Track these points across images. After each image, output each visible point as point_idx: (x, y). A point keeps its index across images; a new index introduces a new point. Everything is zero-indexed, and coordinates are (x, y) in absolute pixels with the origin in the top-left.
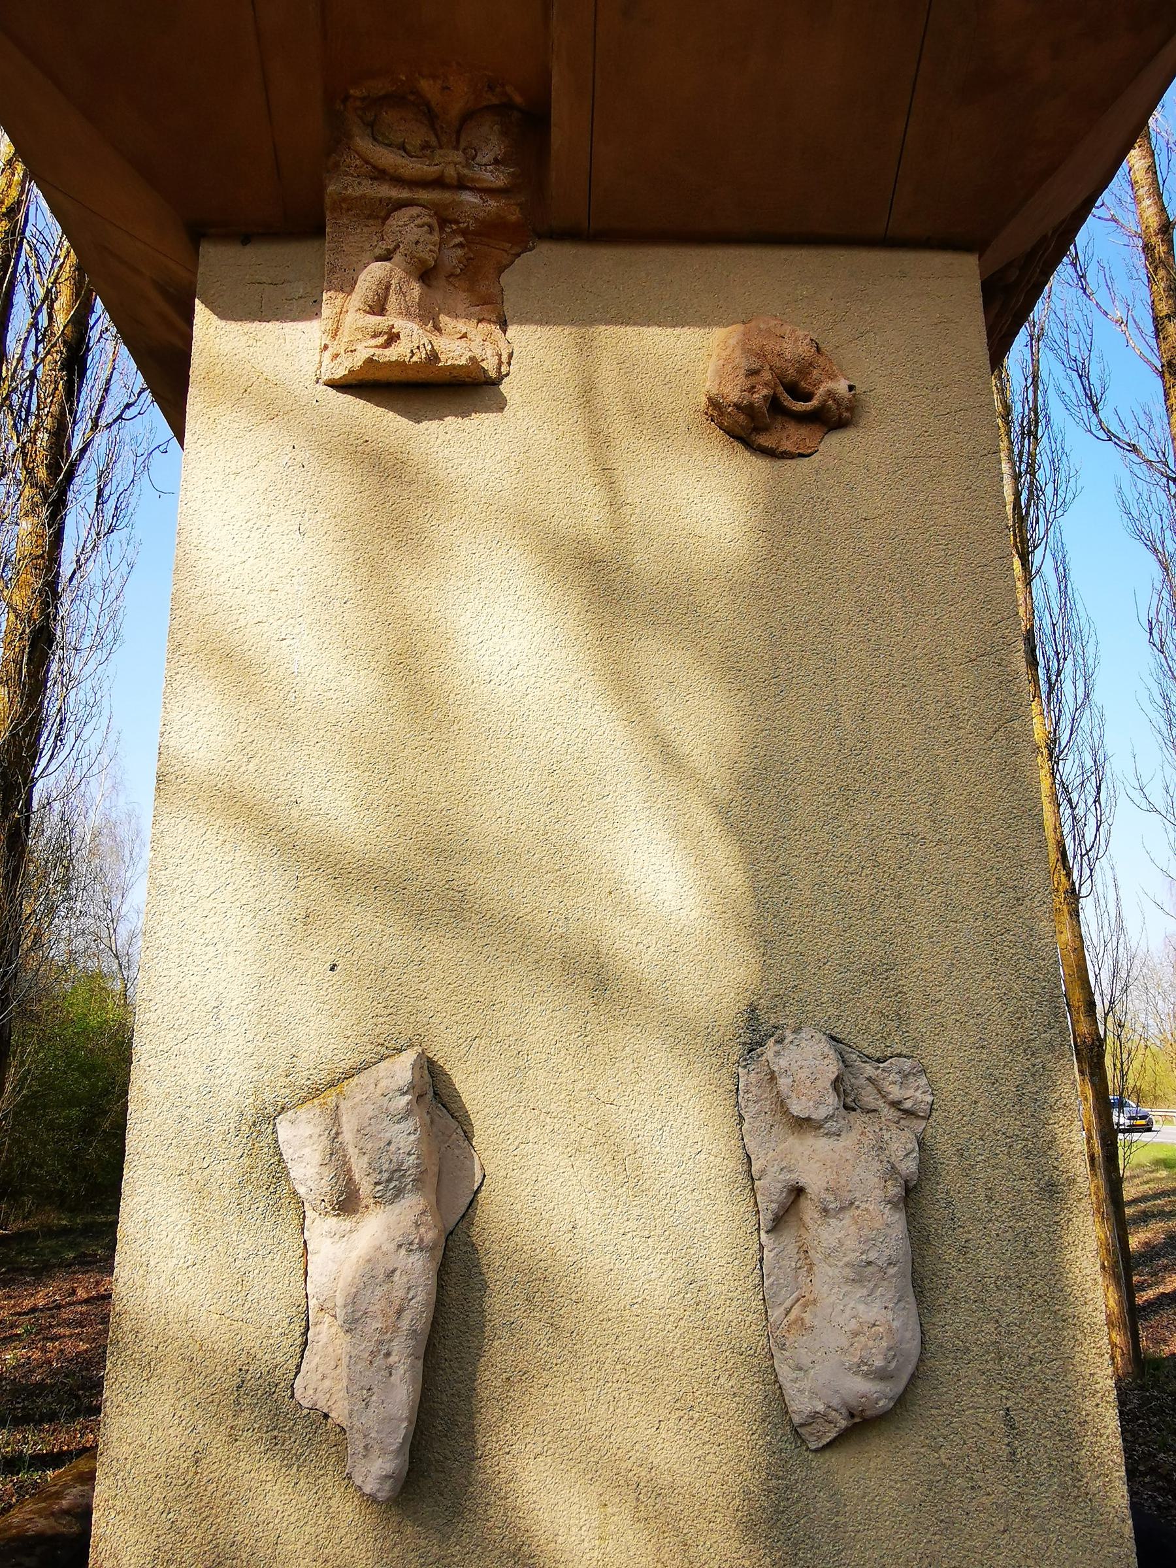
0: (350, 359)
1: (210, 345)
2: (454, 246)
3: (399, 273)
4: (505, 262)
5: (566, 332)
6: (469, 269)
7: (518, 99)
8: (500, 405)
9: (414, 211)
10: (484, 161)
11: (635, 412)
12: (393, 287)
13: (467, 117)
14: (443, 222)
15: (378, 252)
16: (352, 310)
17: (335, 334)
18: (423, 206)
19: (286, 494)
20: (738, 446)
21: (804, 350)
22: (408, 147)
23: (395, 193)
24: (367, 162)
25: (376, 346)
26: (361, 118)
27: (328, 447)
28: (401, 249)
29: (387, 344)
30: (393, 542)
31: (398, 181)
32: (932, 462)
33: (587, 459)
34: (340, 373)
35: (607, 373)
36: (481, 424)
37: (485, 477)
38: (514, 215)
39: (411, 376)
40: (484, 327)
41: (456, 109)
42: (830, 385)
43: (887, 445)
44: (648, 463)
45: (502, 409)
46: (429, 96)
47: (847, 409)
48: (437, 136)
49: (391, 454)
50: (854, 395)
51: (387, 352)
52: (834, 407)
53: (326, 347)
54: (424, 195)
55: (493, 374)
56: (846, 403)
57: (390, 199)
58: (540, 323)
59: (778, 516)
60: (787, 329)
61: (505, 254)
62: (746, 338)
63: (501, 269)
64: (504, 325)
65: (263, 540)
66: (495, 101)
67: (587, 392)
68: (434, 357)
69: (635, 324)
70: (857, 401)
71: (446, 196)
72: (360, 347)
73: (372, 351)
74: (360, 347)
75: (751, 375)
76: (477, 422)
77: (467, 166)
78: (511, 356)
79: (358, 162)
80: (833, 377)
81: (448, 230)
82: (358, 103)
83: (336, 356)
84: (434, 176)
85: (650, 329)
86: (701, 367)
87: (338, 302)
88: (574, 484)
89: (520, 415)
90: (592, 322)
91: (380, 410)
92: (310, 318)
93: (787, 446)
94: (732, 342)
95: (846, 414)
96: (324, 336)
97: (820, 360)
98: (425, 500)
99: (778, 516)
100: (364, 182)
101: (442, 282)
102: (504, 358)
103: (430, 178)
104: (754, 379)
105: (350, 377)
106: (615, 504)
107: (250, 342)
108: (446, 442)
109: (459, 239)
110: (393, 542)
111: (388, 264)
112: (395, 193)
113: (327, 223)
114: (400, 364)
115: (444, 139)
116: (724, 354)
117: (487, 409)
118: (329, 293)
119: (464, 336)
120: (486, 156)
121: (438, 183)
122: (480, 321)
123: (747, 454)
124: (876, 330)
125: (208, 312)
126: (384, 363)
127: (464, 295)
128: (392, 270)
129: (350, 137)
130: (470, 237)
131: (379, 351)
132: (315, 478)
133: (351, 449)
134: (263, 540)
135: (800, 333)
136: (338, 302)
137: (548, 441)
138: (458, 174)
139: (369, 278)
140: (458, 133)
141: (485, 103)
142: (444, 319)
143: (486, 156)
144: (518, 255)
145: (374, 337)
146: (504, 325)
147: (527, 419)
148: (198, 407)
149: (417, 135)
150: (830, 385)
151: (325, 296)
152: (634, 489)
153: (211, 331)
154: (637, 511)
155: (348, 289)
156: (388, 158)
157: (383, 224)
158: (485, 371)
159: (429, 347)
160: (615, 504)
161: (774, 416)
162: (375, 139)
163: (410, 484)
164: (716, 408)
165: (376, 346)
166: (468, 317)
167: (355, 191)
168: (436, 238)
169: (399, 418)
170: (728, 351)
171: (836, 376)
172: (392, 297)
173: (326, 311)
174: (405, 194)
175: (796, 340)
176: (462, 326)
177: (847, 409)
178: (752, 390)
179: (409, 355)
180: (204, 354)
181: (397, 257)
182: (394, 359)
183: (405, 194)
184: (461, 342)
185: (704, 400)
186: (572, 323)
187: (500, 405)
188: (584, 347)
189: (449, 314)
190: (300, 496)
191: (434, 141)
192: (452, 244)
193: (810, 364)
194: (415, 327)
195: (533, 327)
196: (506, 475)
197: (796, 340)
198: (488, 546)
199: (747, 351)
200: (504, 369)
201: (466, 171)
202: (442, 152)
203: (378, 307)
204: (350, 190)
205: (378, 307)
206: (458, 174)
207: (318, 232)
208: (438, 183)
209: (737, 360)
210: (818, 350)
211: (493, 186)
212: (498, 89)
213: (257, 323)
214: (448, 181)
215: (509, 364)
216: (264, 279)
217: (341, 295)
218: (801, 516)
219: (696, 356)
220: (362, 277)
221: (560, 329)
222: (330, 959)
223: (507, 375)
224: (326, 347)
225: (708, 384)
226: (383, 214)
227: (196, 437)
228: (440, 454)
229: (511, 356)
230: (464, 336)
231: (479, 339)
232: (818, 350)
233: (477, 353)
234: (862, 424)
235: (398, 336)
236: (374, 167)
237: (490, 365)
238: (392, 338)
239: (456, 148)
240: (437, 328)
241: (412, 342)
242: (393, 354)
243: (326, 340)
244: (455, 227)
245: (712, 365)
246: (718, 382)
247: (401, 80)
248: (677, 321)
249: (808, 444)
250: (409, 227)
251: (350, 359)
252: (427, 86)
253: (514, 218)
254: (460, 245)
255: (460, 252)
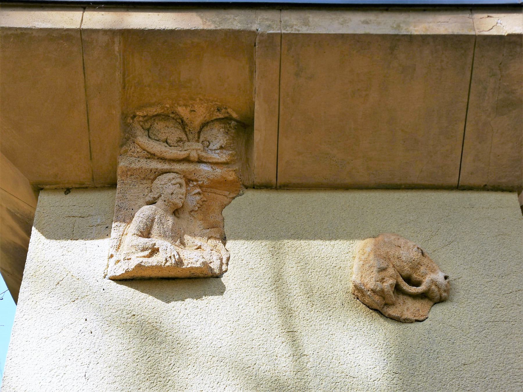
0: (127, 264)
1: (38, 255)
2: (195, 194)
3: (160, 212)
4: (225, 203)
5: (263, 244)
6: (202, 210)
7: (234, 115)
8: (221, 290)
9: (171, 176)
10: (214, 148)
11: (309, 293)
12: (156, 220)
13: (204, 125)
14: (188, 181)
15: (148, 199)
16: (130, 234)
17: (118, 248)
18: (177, 173)
19: (79, 351)
20: (375, 315)
21: (414, 255)
22: (169, 141)
23: (161, 166)
24: (144, 150)
25: (144, 257)
26: (142, 126)
27: (109, 319)
28: (162, 197)
29: (151, 255)
30: (148, 383)
31: (163, 159)
32: (504, 325)
33: (277, 325)
34: (119, 272)
35: (291, 270)
36: (210, 302)
37: (210, 338)
38: (231, 176)
39: (166, 274)
40: (212, 242)
41: (198, 121)
42: (433, 276)
43: (474, 314)
44: (318, 327)
45: (222, 293)
46: (183, 115)
47: (445, 291)
48: (187, 135)
49: (150, 323)
50: (448, 282)
51: (150, 260)
52: (436, 290)
53: (112, 256)
54: (177, 167)
55: (217, 271)
56: (443, 287)
57: (157, 169)
58: (247, 238)
59: (405, 362)
60: (402, 241)
61: (225, 198)
62: (377, 253)
63: (223, 206)
64: (224, 240)
65: (60, 384)
66: (221, 116)
67: (278, 282)
68: (180, 262)
69: (307, 238)
70: (450, 285)
71: (191, 167)
72: (133, 257)
73: (141, 259)
74: (133, 257)
75: (381, 271)
76: (206, 301)
77: (204, 150)
78: (228, 259)
79: (139, 150)
80: (433, 271)
81: (191, 185)
82: (141, 119)
83: (119, 261)
84: (184, 157)
85: (315, 242)
86: (349, 264)
87: (121, 229)
88: (269, 342)
89: (233, 297)
90: (279, 237)
91: (144, 295)
92: (103, 238)
93: (408, 315)
94: (368, 249)
95: (444, 294)
96: (111, 249)
97: (425, 261)
98: (171, 354)
99: (405, 362)
100: (142, 160)
101: (187, 215)
102: (224, 261)
103: (181, 158)
104: (383, 274)
105: (126, 275)
106: (298, 354)
107: (64, 253)
108: (184, 313)
109: (198, 190)
110: (148, 383)
111: (153, 207)
112: (161, 166)
113: (118, 183)
114: (158, 267)
115: (191, 136)
116: (363, 257)
117: (213, 294)
118: (116, 224)
119: (199, 248)
120: (215, 145)
121: (187, 160)
122: (209, 238)
123: (382, 320)
124: (458, 240)
125: (39, 235)
126: (148, 267)
127: (199, 223)
128: (156, 210)
129: (135, 137)
130: (204, 189)
131: (145, 260)
132: (98, 340)
133: (124, 320)
134: (60, 384)
135: (411, 244)
136: (121, 229)
137: (252, 314)
138: (198, 155)
139: (141, 215)
140: (199, 133)
141: (215, 118)
142: (187, 237)
143: (215, 145)
144: (234, 198)
145: (142, 251)
146: (224, 240)
147: (238, 300)
148: (26, 294)
149: (174, 133)
150: (433, 276)
151: (114, 225)
152: (310, 344)
153: (40, 246)
154: (311, 359)
155: (128, 221)
156: (157, 148)
157: (152, 183)
158: (212, 269)
159: (177, 257)
160: (298, 354)
161: (397, 296)
162: (149, 137)
163: (161, 343)
164: (359, 292)
165: (144, 257)
166: (202, 236)
167: (136, 165)
168: (183, 190)
169: (156, 300)
170: (366, 256)
171: (435, 270)
172: (155, 226)
173: (114, 234)
174: (166, 166)
175: (408, 249)
176: (198, 241)
177: (445, 291)
178: (382, 280)
179: (164, 262)
180: (34, 261)
181: (159, 202)
182: (154, 264)
183: (166, 166)
184: (197, 253)
185: (351, 286)
186: (267, 238)
187: (221, 290)
188: (275, 253)
189: (190, 234)
190: (88, 352)
191: (184, 137)
192: (194, 193)
193: (419, 263)
194: (169, 244)
195: (242, 241)
196: (224, 336)
197: (408, 249)
198: (211, 385)
199: (378, 256)
200: (224, 268)
201: (204, 154)
202: (189, 144)
203: (146, 233)
204: (133, 165)
205: (146, 233)
206: (198, 155)
207: (113, 185)
208: (187, 160)
209: (372, 262)
210: (423, 253)
211: (220, 161)
212: (223, 111)
213: (69, 241)
214: (192, 159)
215: (227, 264)
216: (76, 214)
217: (124, 224)
218: (420, 363)
219: (347, 259)
220: (137, 215)
221: (259, 242)
222: (85, 317)
223: (226, 271)
224: (112, 256)
225: (354, 276)
226: (152, 177)
227: (22, 314)
228: (182, 323)
229: (228, 259)
230: (199, 248)
231: (208, 250)
232: (423, 253)
233: (207, 258)
234: (455, 300)
235: (158, 250)
236: (148, 152)
237: (215, 266)
238: (154, 251)
239: (198, 141)
240: (183, 243)
241: (166, 252)
242: (154, 261)
243: (112, 251)
244: (195, 183)
245: (356, 264)
246: (360, 275)
247: (166, 107)
248: (332, 235)
249: (421, 313)
250: (169, 185)
251: (127, 264)
252: (182, 111)
253: (231, 178)
254: (199, 193)
255: (198, 197)
